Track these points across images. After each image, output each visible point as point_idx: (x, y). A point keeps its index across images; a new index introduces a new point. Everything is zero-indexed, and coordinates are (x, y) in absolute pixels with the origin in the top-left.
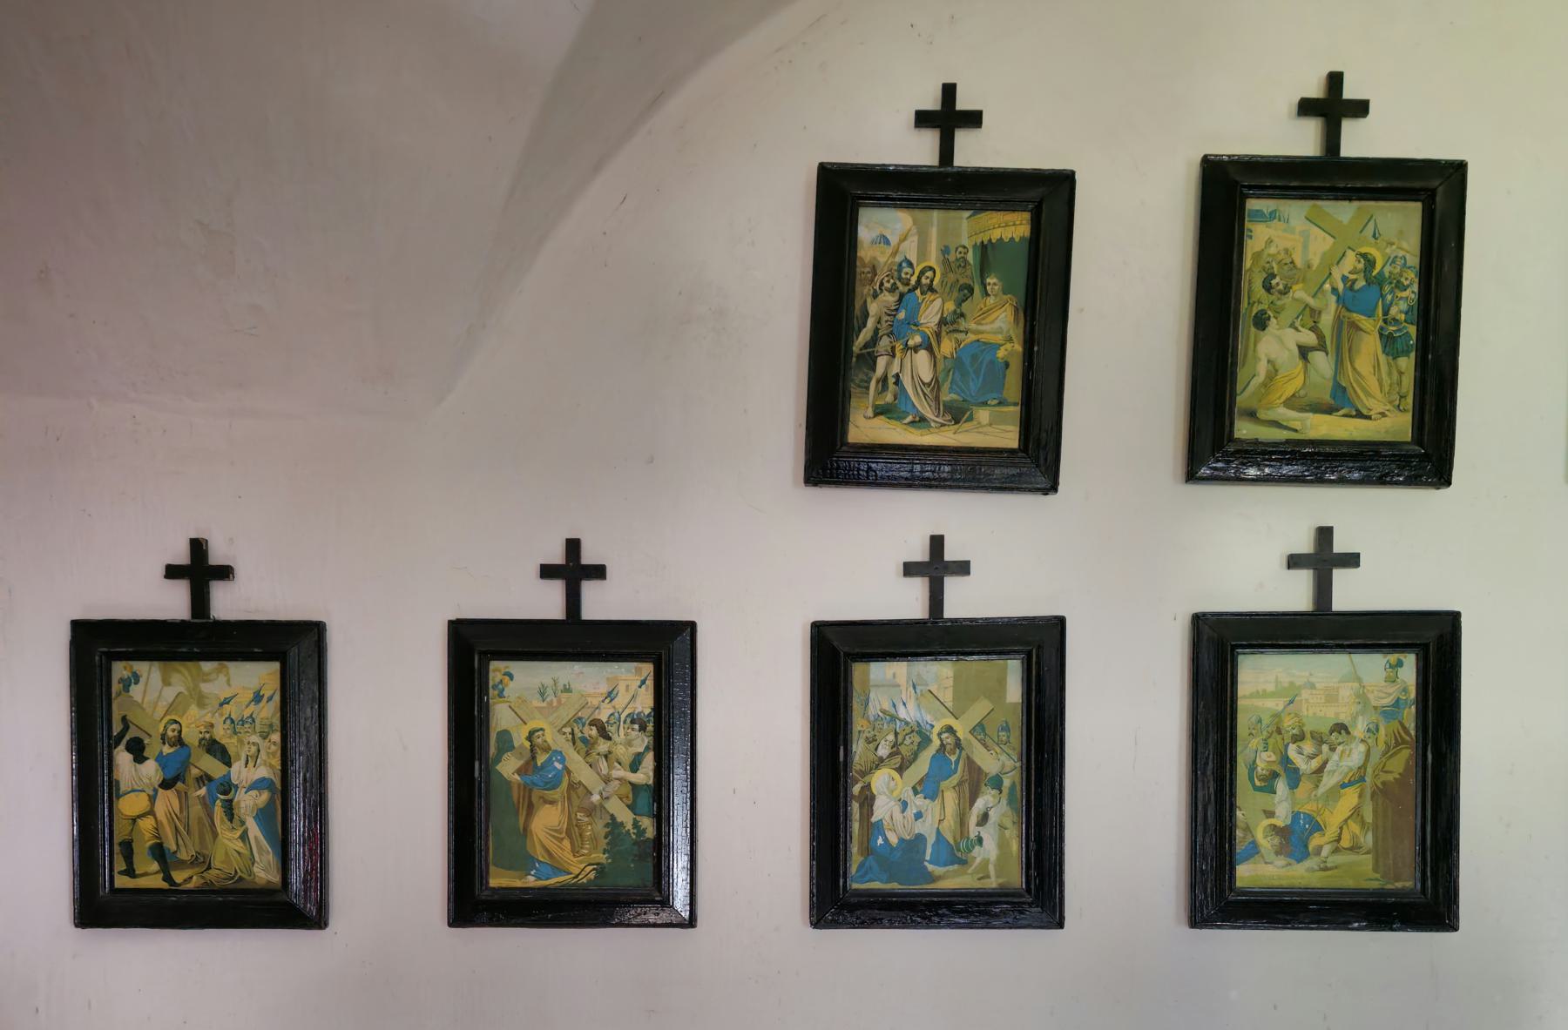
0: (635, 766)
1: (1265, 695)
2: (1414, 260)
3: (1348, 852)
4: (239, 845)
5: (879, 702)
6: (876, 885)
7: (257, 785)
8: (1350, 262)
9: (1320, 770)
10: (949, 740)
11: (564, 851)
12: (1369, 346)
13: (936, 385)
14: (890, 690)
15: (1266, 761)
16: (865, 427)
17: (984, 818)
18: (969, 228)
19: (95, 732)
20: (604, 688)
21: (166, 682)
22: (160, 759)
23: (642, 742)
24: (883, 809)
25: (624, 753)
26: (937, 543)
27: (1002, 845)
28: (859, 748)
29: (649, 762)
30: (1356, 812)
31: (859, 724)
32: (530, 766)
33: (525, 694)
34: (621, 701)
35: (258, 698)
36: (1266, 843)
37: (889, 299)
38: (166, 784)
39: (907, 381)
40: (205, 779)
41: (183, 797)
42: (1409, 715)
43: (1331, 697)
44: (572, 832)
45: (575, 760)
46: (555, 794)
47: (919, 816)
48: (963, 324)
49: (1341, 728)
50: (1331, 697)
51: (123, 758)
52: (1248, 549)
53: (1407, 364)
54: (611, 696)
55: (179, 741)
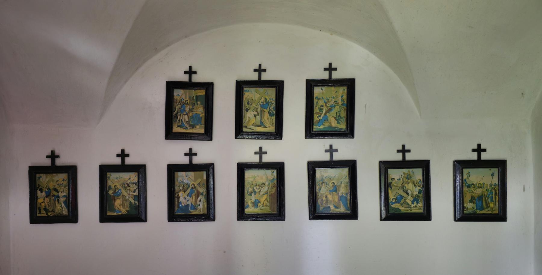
0: (134, 192)
1: (249, 178)
2: (274, 99)
3: (265, 207)
4: (60, 208)
5: (180, 179)
6: (180, 214)
7: (64, 196)
8: (263, 99)
9: (260, 191)
10: (193, 186)
11: (121, 208)
12: (266, 115)
13: (189, 121)
14: (182, 177)
15: (250, 190)
16: (176, 129)
17: (200, 201)
18: (194, 93)
19: (34, 187)
20: (128, 177)
21: (47, 178)
22: (46, 192)
23: (135, 187)
24: (181, 199)
25: (132, 189)
26: (261, 148)
27: (203, 205)
28: (177, 188)
29: (137, 191)
30: (266, 199)
31: (176, 183)
32: (114, 192)
33: (114, 178)
34: (132, 180)
35: (63, 180)
36: (250, 205)
37: (180, 106)
38: (47, 197)
39: (183, 121)
40: (54, 196)
41: (50, 199)
42: (275, 181)
43: (262, 178)
44: (123, 204)
45: (123, 191)
46: (119, 197)
47: (188, 200)
48: (194, 110)
49: (263, 184)
50: (262, 178)
51: (39, 192)
52: (318, 149)
53: (274, 118)
54: (130, 179)
55: (49, 189)
